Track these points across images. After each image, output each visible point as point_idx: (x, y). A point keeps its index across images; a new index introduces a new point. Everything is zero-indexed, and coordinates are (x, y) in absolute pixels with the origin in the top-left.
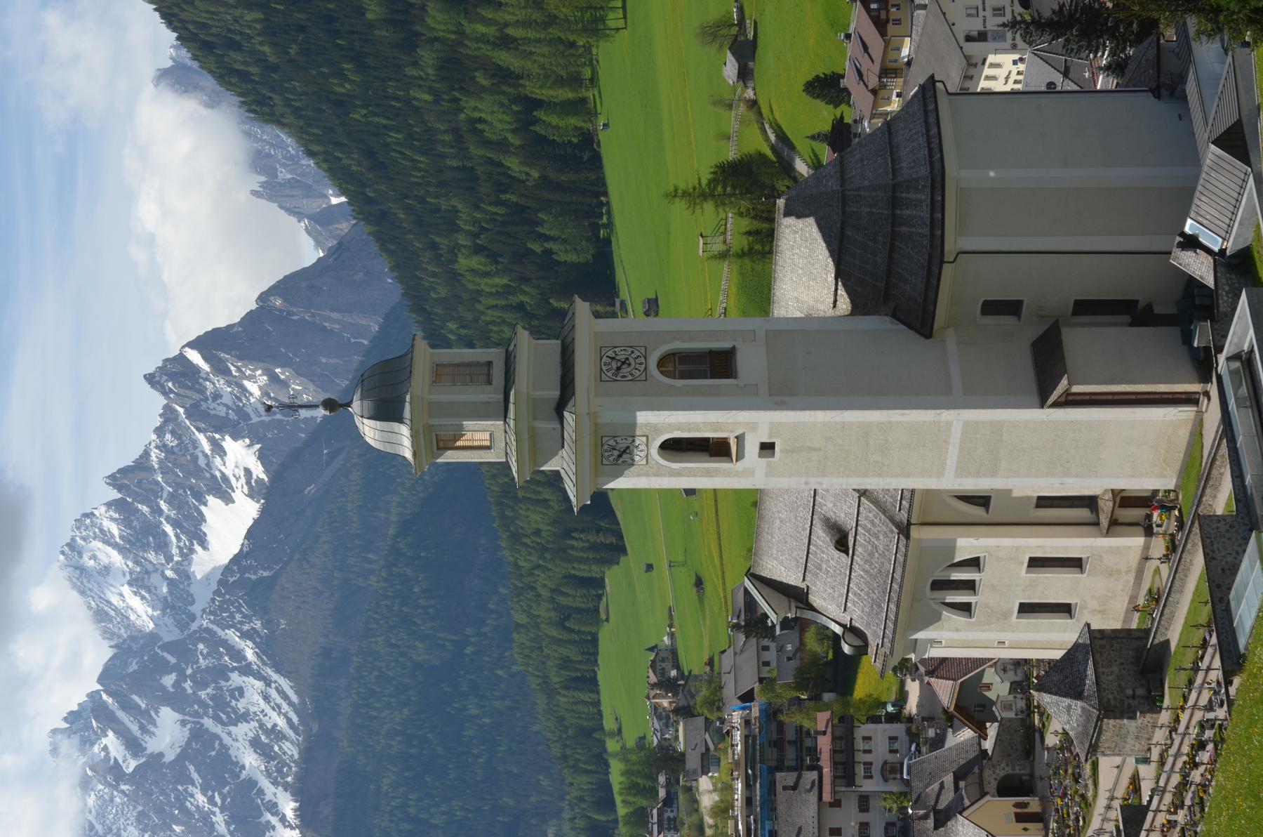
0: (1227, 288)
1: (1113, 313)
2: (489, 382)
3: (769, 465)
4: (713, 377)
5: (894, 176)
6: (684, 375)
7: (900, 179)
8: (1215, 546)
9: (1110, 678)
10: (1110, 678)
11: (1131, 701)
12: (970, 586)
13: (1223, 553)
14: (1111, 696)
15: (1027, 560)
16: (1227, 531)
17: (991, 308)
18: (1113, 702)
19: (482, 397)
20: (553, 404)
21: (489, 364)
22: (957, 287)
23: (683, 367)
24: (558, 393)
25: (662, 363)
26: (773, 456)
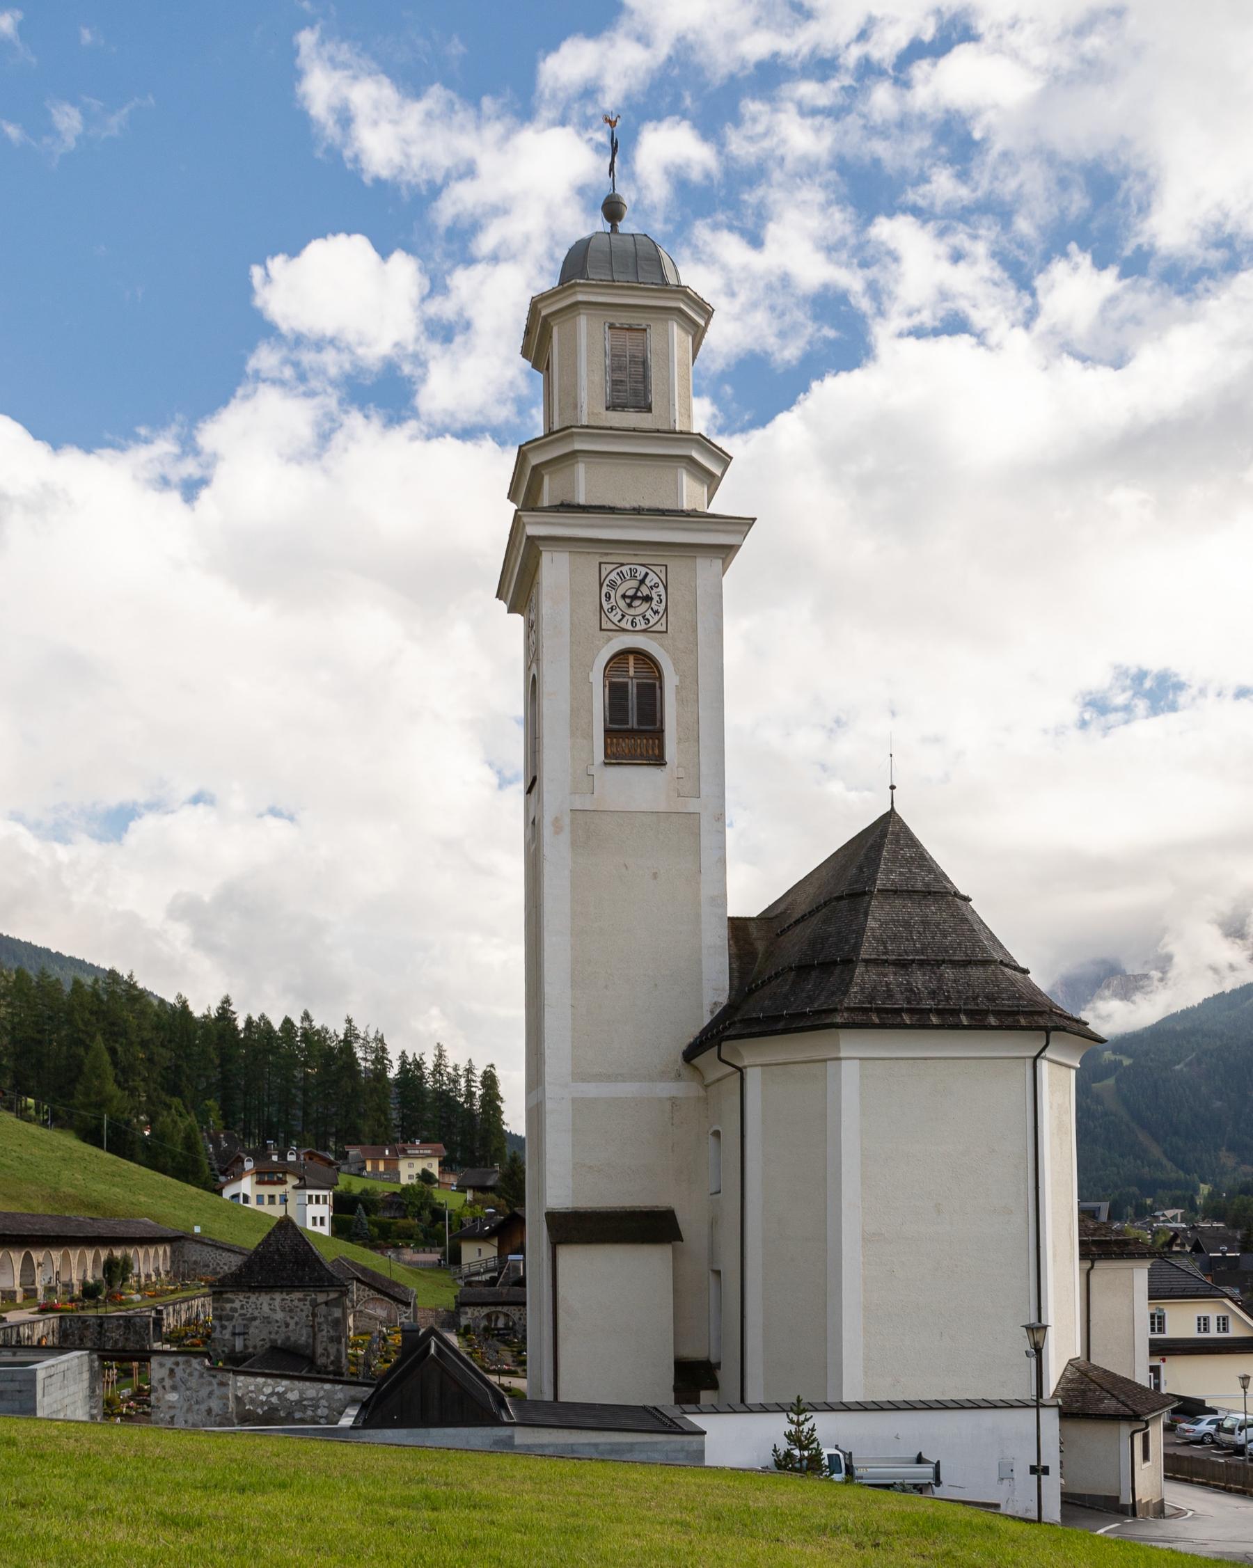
0: (293, 1396)
4: (607, 732)
9: (266, 1308)
11: (229, 1329)
14: (237, 1305)
19: (584, 397)
20: (568, 499)
21: (649, 409)
23: (633, 691)
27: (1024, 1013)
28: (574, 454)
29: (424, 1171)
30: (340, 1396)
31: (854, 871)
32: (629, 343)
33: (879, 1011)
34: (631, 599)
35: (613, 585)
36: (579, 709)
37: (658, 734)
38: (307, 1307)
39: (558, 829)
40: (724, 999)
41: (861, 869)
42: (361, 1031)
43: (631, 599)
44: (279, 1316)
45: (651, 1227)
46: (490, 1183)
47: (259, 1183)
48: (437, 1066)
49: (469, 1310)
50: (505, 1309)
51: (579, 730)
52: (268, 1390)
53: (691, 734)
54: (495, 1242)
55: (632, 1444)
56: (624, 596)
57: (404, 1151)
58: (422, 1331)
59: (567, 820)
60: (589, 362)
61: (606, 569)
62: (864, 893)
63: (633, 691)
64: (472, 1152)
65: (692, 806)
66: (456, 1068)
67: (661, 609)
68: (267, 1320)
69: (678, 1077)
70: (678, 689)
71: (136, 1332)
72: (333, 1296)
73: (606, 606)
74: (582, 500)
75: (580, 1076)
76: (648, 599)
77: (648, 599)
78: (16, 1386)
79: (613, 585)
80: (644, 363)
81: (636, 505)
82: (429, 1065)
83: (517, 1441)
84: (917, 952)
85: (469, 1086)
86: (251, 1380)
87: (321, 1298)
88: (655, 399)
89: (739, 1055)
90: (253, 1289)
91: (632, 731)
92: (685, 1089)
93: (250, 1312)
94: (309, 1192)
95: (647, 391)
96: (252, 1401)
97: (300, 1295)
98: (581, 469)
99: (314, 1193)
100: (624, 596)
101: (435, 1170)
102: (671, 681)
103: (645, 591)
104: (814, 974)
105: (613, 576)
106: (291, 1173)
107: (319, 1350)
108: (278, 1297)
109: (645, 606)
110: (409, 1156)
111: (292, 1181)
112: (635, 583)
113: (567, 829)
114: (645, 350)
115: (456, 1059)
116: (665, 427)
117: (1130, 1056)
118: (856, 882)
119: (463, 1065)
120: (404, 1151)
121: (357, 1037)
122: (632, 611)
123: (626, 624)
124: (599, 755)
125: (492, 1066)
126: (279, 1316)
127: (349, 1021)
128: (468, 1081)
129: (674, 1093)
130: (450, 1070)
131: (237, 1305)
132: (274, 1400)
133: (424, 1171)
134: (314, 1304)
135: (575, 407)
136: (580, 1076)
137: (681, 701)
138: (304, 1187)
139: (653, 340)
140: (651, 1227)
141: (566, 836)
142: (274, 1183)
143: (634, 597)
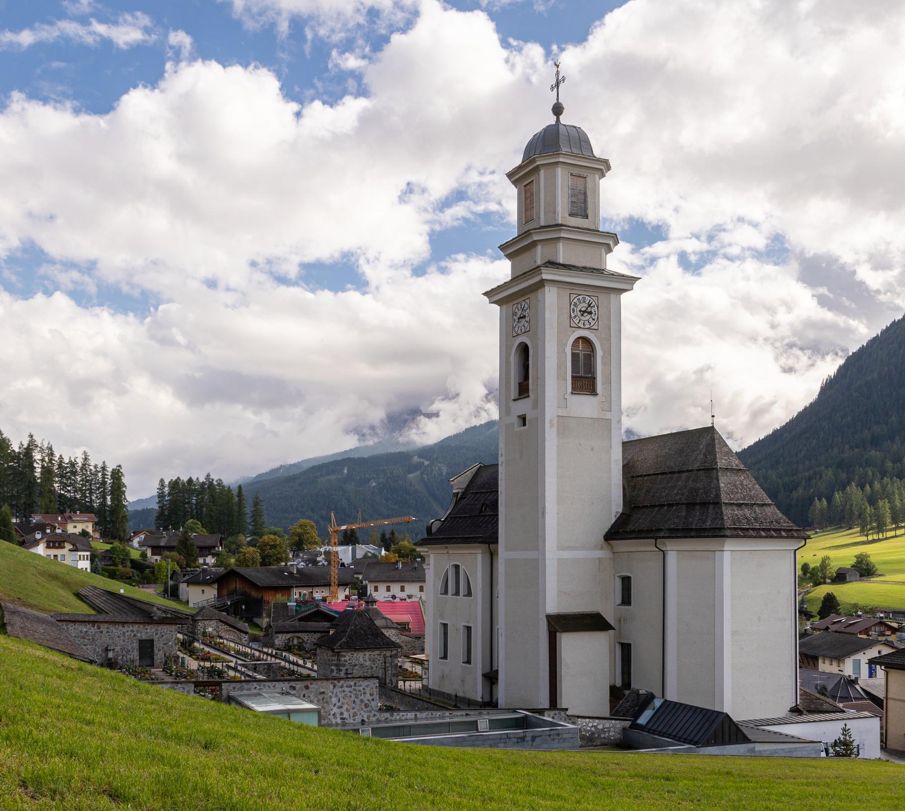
0: (600, 727)
1: (623, 673)
2: (571, 215)
3: (513, 424)
4: (573, 377)
5: (726, 504)
6: (575, 356)
7: (724, 508)
8: (346, 689)
9: (361, 659)
10: (361, 659)
11: (344, 671)
12: (457, 593)
13: (340, 695)
14: (347, 658)
15: (470, 625)
16: (362, 701)
17: (626, 582)
18: (343, 659)
19: (559, 209)
20: (553, 259)
21: (587, 217)
22: (640, 556)
23: (581, 357)
24: (561, 262)
25: (586, 341)
26: (519, 427)
27: (784, 530)
28: (559, 238)
29: (83, 530)
30: (618, 726)
31: (702, 456)
32: (579, 183)
33: (742, 529)
34: (583, 312)
35: (575, 305)
36: (561, 365)
37: (593, 379)
38: (382, 659)
39: (552, 426)
40: (620, 510)
41: (705, 455)
42: (39, 442)
43: (583, 312)
44: (368, 663)
45: (592, 622)
46: (162, 544)
47: (48, 547)
48: (84, 465)
49: (280, 636)
50: (299, 635)
51: (561, 376)
52: (590, 725)
53: (608, 381)
54: (216, 586)
55: (796, 748)
56: (580, 311)
57: (70, 518)
58: (180, 636)
59: (555, 421)
60: (562, 191)
61: (573, 296)
62: (713, 469)
63: (581, 357)
64: (105, 518)
65: (608, 415)
66: (96, 467)
67: (596, 318)
68: (362, 666)
69: (602, 548)
70: (603, 358)
71: (274, 672)
72: (394, 652)
73: (573, 315)
74: (561, 261)
75: (561, 548)
76: (590, 313)
77: (590, 313)
78: (570, 736)
79: (575, 305)
80: (585, 194)
81: (583, 265)
82: (80, 462)
83: (756, 749)
84: (744, 499)
85: (104, 478)
86: (584, 720)
87: (388, 653)
88: (590, 212)
89: (665, 544)
90: (356, 650)
91: (581, 377)
92: (603, 554)
93: (354, 662)
94: (79, 553)
95: (586, 208)
96: (585, 730)
97: (378, 652)
98: (561, 245)
99: (82, 553)
100: (580, 311)
101: (90, 530)
102: (599, 354)
103: (589, 309)
104: (698, 507)
105: (575, 300)
106: (68, 542)
107: (388, 681)
108: (367, 653)
109: (589, 316)
110: (74, 521)
111: (68, 546)
112: (586, 305)
113: (555, 425)
114: (585, 187)
115: (95, 461)
116: (592, 227)
117: (428, 460)
118: (705, 462)
119: (100, 465)
120: (70, 518)
121: (37, 446)
122: (582, 318)
123: (581, 325)
124: (569, 389)
125: (120, 466)
126: (368, 663)
127: (31, 436)
128: (104, 475)
129: (600, 556)
130: (92, 468)
131: (347, 658)
132: (593, 729)
133: (83, 530)
134: (385, 657)
135: (555, 213)
136: (561, 548)
137: (604, 364)
138: (77, 550)
139: (589, 184)
140: (592, 622)
141: (555, 429)
142: (57, 548)
143: (584, 312)
